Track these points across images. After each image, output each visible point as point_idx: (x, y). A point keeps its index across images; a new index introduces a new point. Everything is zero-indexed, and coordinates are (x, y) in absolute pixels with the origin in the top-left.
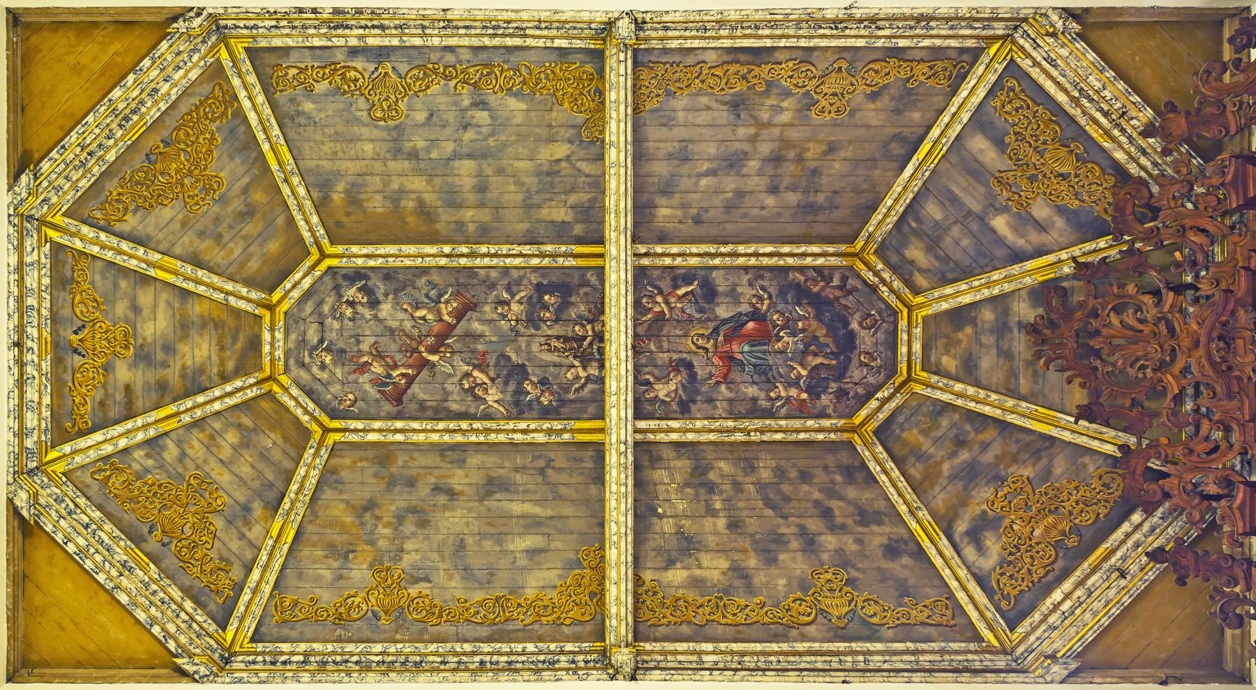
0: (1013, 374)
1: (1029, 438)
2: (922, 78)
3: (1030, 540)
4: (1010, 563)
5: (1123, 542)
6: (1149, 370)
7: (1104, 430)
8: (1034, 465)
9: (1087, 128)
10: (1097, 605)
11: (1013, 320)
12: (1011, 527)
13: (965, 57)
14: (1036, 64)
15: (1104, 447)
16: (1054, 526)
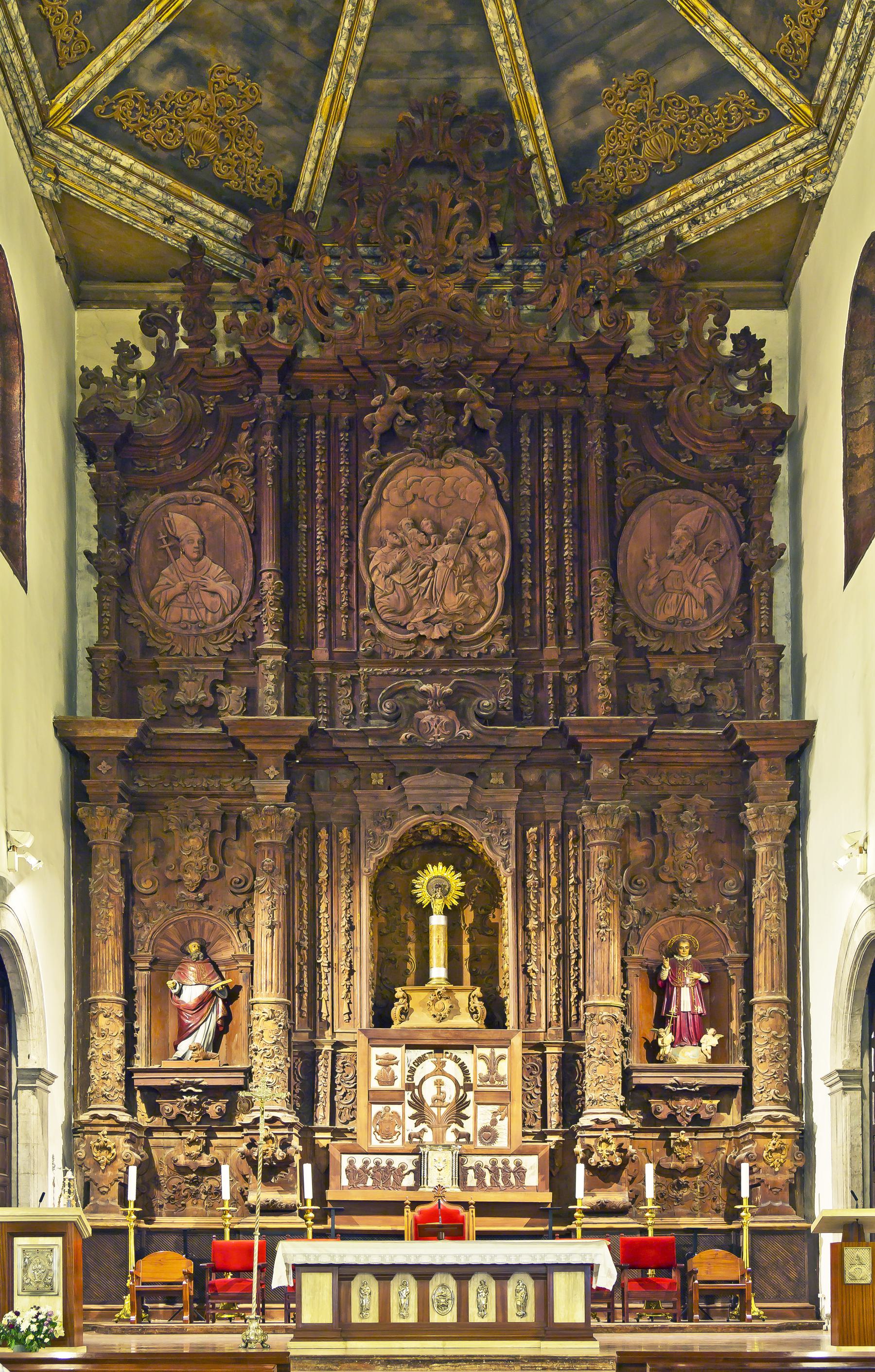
0: (391, 71)
1: (309, 95)
2: (792, 32)
3: (184, 120)
4: (151, 104)
8: (276, 107)
10: (127, 203)
11: (462, 72)
12: (196, 97)
13: (805, 81)
15: (308, 173)
16: (206, 140)
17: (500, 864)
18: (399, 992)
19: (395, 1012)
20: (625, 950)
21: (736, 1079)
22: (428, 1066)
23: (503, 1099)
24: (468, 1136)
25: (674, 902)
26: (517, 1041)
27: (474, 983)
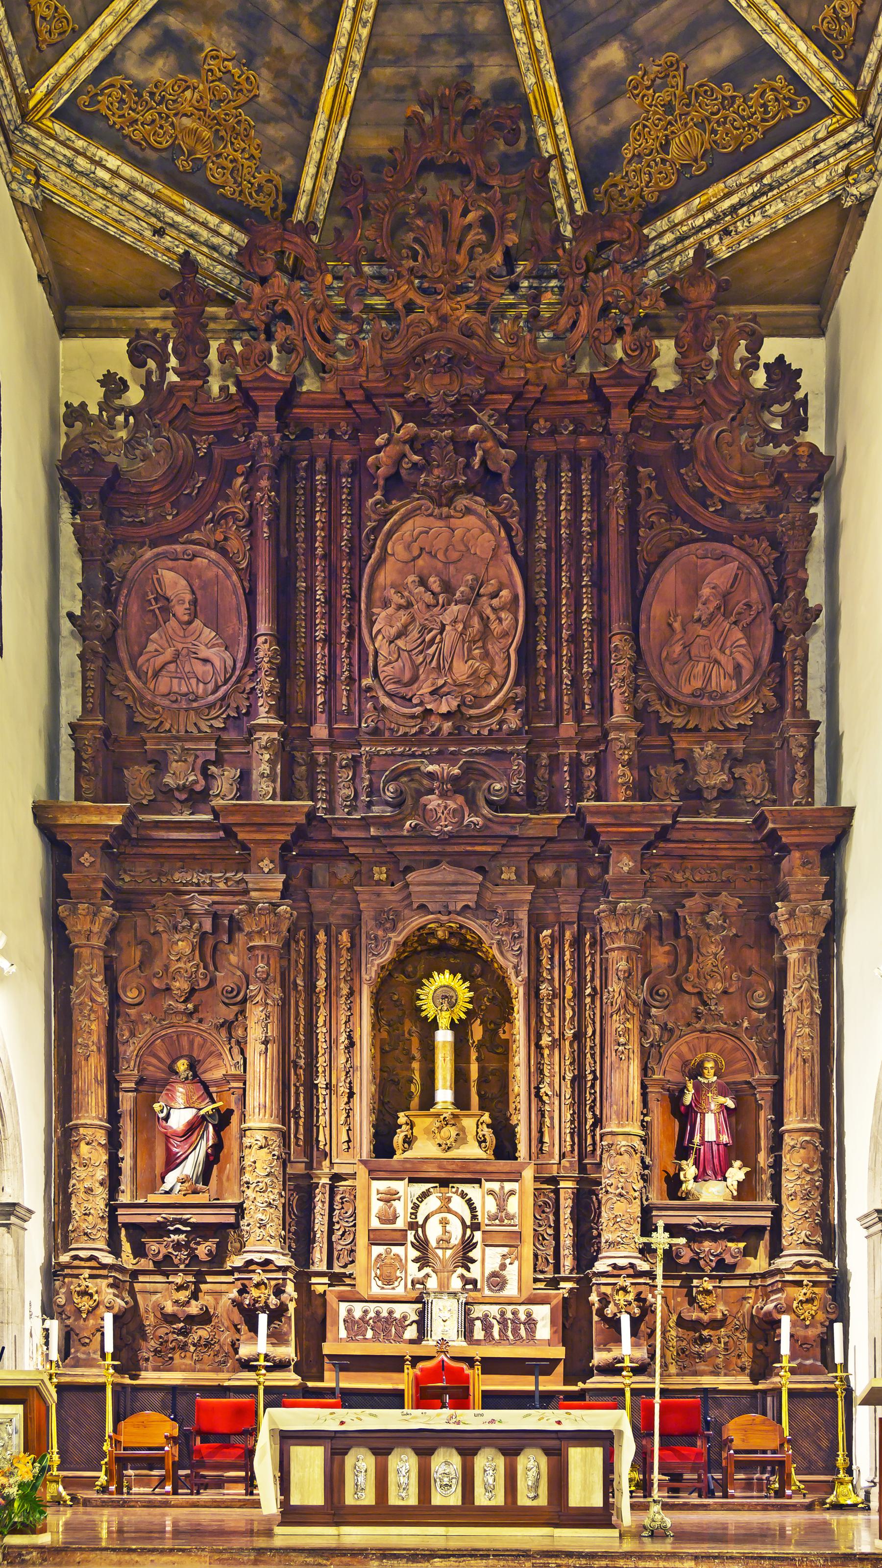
1: (310, 87)
3: (175, 115)
4: (139, 95)
5: (195, 221)
6: (412, 263)
7: (330, 177)
8: (275, 100)
9: (722, 185)
10: (114, 211)
11: (475, 58)
12: (188, 88)
13: (850, 62)
14: (816, 143)
16: (199, 140)
17: (511, 972)
18: (402, 1118)
19: (398, 1139)
20: (645, 1070)
21: (764, 1219)
22: (433, 1203)
23: (514, 1239)
24: (474, 1282)
25: (698, 1016)
26: (528, 1174)
27: (482, 1108)
